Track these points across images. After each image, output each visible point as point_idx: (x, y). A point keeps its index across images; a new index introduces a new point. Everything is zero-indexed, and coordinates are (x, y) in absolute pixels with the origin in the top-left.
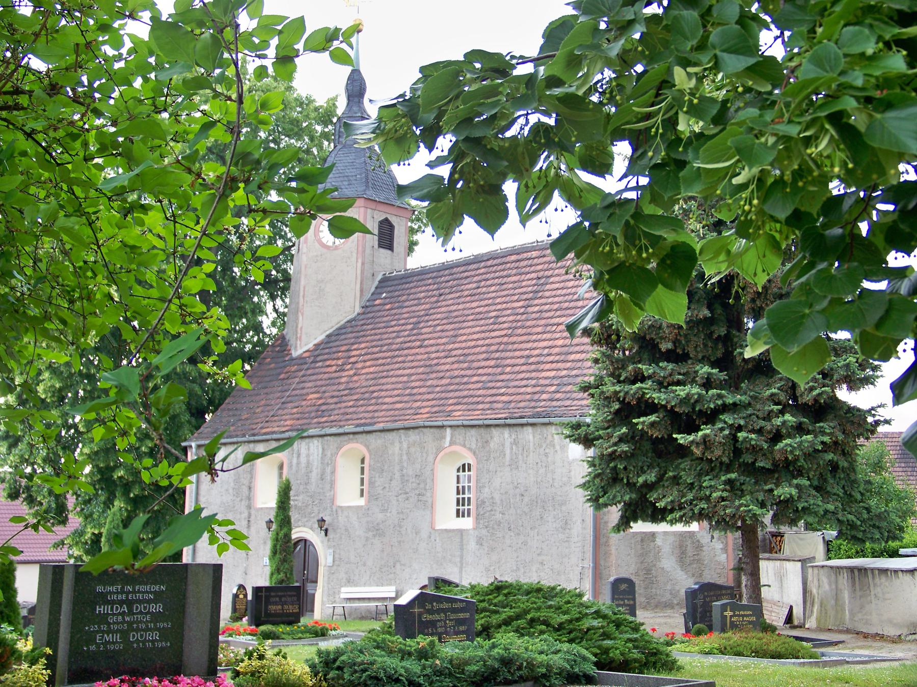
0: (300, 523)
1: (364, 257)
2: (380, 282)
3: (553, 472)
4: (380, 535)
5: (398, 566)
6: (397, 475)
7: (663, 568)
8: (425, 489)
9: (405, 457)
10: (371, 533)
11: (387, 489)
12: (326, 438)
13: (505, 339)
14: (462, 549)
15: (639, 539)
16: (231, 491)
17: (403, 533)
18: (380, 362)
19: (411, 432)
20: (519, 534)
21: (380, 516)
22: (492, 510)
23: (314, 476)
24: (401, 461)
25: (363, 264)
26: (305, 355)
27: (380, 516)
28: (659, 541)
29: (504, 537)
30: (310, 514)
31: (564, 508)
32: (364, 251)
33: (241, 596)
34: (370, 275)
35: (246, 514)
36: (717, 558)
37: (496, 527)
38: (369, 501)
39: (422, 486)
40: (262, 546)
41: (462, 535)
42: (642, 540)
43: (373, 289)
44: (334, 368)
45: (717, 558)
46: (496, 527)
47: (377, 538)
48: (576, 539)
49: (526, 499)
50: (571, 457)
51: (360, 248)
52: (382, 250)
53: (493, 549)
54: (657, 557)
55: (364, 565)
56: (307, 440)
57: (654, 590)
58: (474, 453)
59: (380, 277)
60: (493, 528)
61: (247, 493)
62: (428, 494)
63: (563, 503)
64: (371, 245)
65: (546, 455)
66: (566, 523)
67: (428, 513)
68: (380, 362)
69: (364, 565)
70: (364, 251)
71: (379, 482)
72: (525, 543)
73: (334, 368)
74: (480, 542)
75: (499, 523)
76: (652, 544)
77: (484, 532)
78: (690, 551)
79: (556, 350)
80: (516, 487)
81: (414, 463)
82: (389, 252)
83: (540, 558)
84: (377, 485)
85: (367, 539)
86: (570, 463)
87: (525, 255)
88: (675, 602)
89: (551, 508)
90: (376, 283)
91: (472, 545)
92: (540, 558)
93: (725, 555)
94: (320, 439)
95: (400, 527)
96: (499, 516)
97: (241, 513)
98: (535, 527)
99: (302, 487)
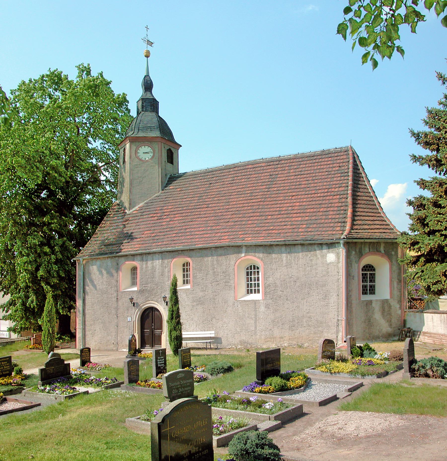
0: (149, 299)
1: (162, 166)
2: (169, 178)
3: (316, 269)
4: (201, 304)
5: (214, 320)
6: (211, 272)
7: (375, 318)
8: (229, 279)
9: (215, 263)
10: (195, 303)
11: (205, 280)
12: (164, 253)
13: (261, 203)
14: (255, 311)
15: (365, 303)
16: (105, 283)
17: (216, 302)
18: (184, 214)
19: (219, 249)
20: (293, 302)
21: (201, 294)
22: (275, 290)
23: (157, 274)
24: (213, 265)
25: (161, 169)
26: (134, 212)
27: (201, 294)
28: (374, 305)
29: (283, 304)
30: (156, 293)
31: (324, 288)
32: (162, 163)
33: (134, 341)
34: (164, 175)
35: (115, 295)
36: (397, 312)
37: (278, 298)
38: (193, 286)
39: (227, 277)
40: (126, 312)
41: (255, 303)
42: (367, 304)
43: (166, 182)
44: (156, 218)
45: (397, 312)
46: (278, 298)
47: (199, 306)
48: (333, 305)
49: (298, 284)
50: (328, 261)
51: (160, 162)
52: (168, 163)
53: (276, 310)
54: (373, 313)
55: (192, 319)
56: (152, 255)
57: (372, 330)
58: (262, 260)
59: (168, 176)
60: (276, 299)
61: (115, 284)
62: (232, 282)
63: (324, 285)
64: (164, 161)
65: (311, 260)
66: (326, 296)
67: (233, 292)
68: (184, 214)
69: (192, 319)
70: (162, 163)
71: (199, 275)
72: (298, 307)
73: (156, 218)
74: (267, 306)
75: (280, 297)
76: (370, 306)
77: (270, 301)
78: (386, 308)
79: (284, 209)
80: (291, 278)
81: (221, 266)
82: (172, 165)
83: (308, 315)
84: (198, 277)
85: (193, 306)
86: (328, 264)
87: (257, 165)
88: (380, 335)
89: (315, 288)
90: (168, 179)
91: (262, 308)
92: (308, 315)
93: (400, 310)
94: (160, 254)
95: (214, 299)
96: (280, 293)
97: (112, 294)
98: (304, 299)
99: (149, 280)
